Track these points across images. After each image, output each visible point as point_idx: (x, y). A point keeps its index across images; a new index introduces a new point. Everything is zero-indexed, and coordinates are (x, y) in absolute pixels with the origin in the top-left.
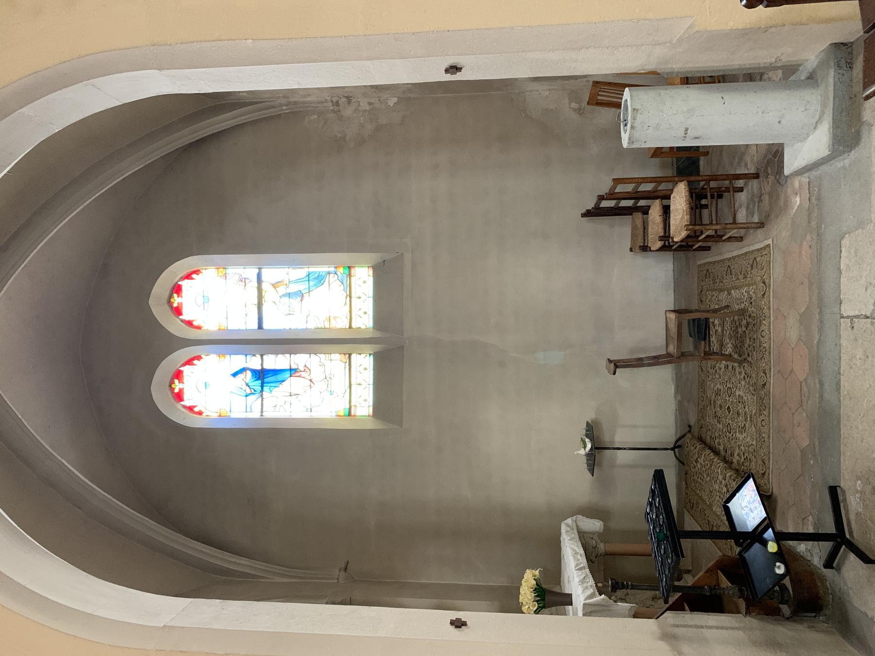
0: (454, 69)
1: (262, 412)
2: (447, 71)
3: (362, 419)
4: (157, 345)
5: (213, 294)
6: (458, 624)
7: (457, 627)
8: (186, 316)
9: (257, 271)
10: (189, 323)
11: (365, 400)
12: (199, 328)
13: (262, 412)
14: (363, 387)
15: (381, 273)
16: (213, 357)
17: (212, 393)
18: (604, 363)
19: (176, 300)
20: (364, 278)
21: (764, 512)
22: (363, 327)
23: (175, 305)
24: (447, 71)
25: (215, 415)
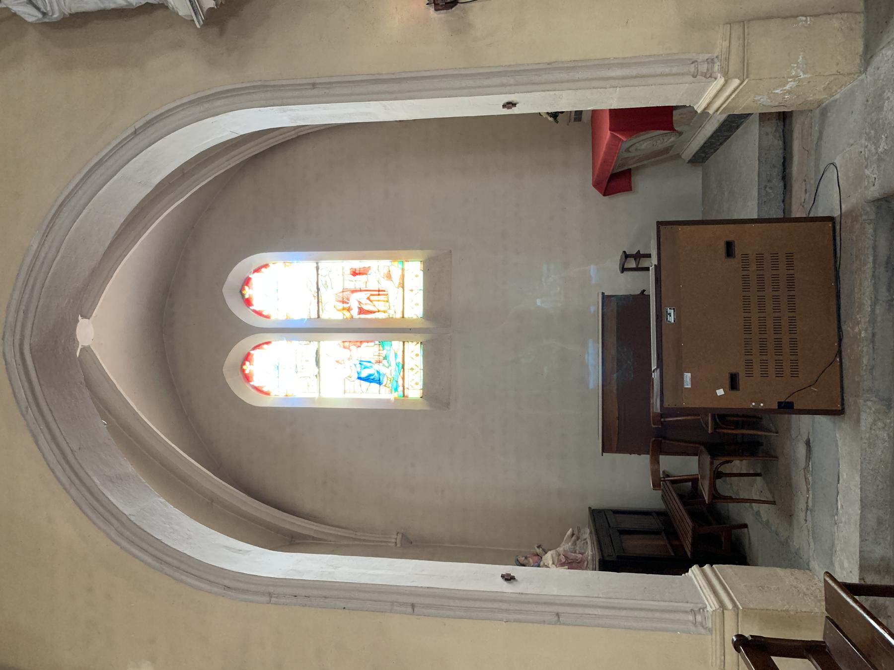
0: (510, 105)
1: (317, 268)
2: (504, 106)
3: (414, 402)
4: (235, 330)
5: (280, 284)
6: (508, 578)
7: (506, 580)
8: (256, 382)
9: (315, 265)
10: (259, 313)
11: (417, 384)
12: (268, 317)
13: (317, 268)
14: (415, 371)
15: (428, 270)
16: (280, 264)
17: (280, 375)
18: (621, 253)
19: (248, 367)
20: (413, 271)
21: (799, 408)
22: (415, 317)
23: (247, 296)
24: (504, 106)
25: (282, 395)
